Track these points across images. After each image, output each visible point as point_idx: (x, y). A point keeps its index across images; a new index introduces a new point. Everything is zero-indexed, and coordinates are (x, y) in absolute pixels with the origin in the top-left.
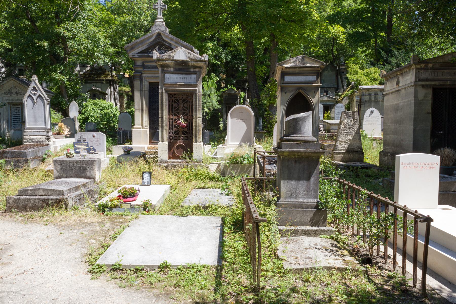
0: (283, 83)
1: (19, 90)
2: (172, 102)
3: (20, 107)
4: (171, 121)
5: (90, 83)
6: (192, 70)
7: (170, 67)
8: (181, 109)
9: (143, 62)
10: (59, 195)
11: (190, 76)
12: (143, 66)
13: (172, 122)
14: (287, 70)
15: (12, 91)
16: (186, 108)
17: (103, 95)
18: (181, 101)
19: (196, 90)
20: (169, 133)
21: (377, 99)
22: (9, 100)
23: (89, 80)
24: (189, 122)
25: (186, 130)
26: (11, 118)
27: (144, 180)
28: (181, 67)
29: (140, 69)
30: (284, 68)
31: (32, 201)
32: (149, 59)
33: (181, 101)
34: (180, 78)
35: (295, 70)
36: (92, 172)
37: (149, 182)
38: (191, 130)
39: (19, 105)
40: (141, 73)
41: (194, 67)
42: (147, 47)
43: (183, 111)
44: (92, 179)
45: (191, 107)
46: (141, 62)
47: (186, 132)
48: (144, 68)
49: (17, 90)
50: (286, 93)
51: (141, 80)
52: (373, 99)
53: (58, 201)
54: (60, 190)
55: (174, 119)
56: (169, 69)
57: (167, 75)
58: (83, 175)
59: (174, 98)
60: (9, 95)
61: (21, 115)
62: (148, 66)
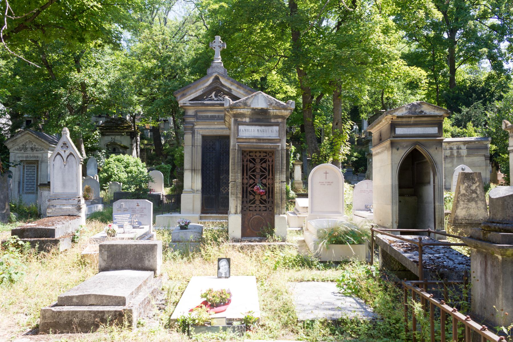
0: (394, 137)
1: (35, 145)
2: (247, 161)
3: (36, 165)
4: (245, 186)
5: (108, 135)
6: (273, 121)
7: (245, 117)
8: (258, 170)
9: (196, 112)
10: (118, 304)
11: (270, 128)
12: (196, 116)
13: (247, 187)
14: (400, 120)
15: (27, 147)
16: (265, 169)
17: (126, 150)
18: (258, 160)
19: (279, 146)
21: (460, 154)
22: (22, 157)
23: (107, 132)
24: (269, 188)
25: (264, 197)
26: (23, 179)
27: (220, 270)
28: (259, 117)
29: (192, 120)
30: (394, 118)
31: (79, 315)
32: (204, 107)
33: (258, 160)
34: (258, 130)
35: (409, 120)
36: (151, 260)
37: (228, 273)
38: (271, 198)
39: (34, 163)
40: (193, 124)
41: (277, 117)
42: (202, 93)
43: (255, 173)
44: (151, 270)
45: (271, 167)
46: (194, 111)
47: (265, 201)
48: (197, 119)
49: (33, 146)
50: (398, 149)
51: (193, 133)
52: (456, 154)
53: (118, 313)
54: (120, 297)
56: (244, 120)
57: (241, 127)
58: (140, 265)
59: (250, 156)
60: (23, 151)
61: (35, 176)
62: (202, 116)
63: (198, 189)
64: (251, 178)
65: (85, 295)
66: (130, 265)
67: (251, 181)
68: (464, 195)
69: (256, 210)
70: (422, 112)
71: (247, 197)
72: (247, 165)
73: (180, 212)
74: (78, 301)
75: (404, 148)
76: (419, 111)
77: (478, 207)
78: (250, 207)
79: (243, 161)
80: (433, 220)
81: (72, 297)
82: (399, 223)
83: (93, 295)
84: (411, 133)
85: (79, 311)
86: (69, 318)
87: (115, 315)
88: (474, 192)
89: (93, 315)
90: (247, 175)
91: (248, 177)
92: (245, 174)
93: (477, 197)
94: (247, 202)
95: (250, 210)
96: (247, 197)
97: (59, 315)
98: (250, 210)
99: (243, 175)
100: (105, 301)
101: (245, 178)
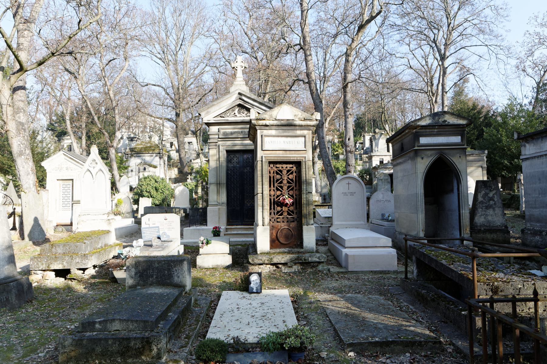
2: (274, 173)
4: (272, 198)
8: (285, 182)
18: (285, 172)
20: (270, 214)
33: (285, 172)
43: (282, 185)
50: (422, 158)
55: (276, 196)
59: (276, 167)
63: (223, 201)
64: (278, 190)
67: (279, 193)
68: (482, 202)
69: (283, 222)
70: (445, 121)
71: (274, 209)
72: (273, 177)
73: (206, 225)
74: (101, 327)
75: (428, 157)
76: (443, 120)
77: (496, 214)
78: (277, 218)
79: (270, 173)
80: (458, 227)
82: (425, 231)
84: (435, 142)
88: (492, 199)
90: (274, 187)
91: (275, 189)
92: (272, 186)
93: (495, 204)
94: (274, 213)
95: (277, 222)
96: (274, 209)
98: (277, 222)
99: (270, 186)
101: (272, 190)
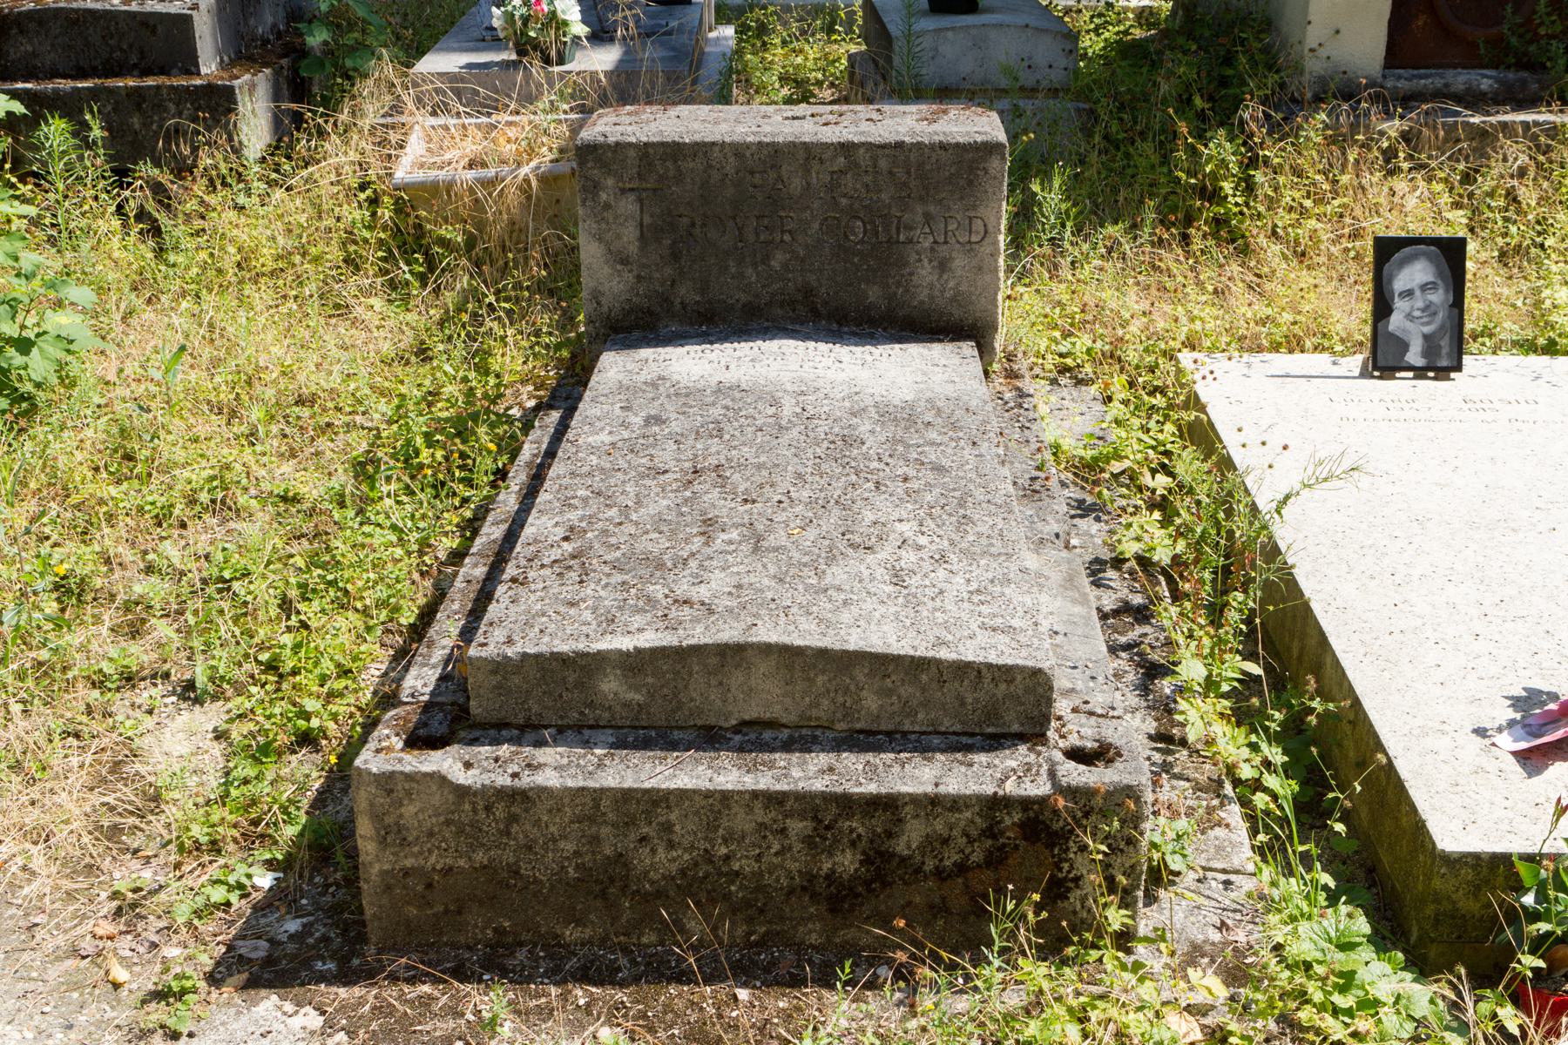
27: (1396, 322)
36: (959, 262)
37: (1445, 344)
53: (1011, 819)
54: (1006, 673)
58: (873, 294)
65: (697, 650)
66: (808, 292)
81: (586, 666)
83: (767, 649)
85: (682, 794)
86: (595, 840)
87: (991, 832)
89: (797, 827)
97: (513, 819)
100: (871, 702)
